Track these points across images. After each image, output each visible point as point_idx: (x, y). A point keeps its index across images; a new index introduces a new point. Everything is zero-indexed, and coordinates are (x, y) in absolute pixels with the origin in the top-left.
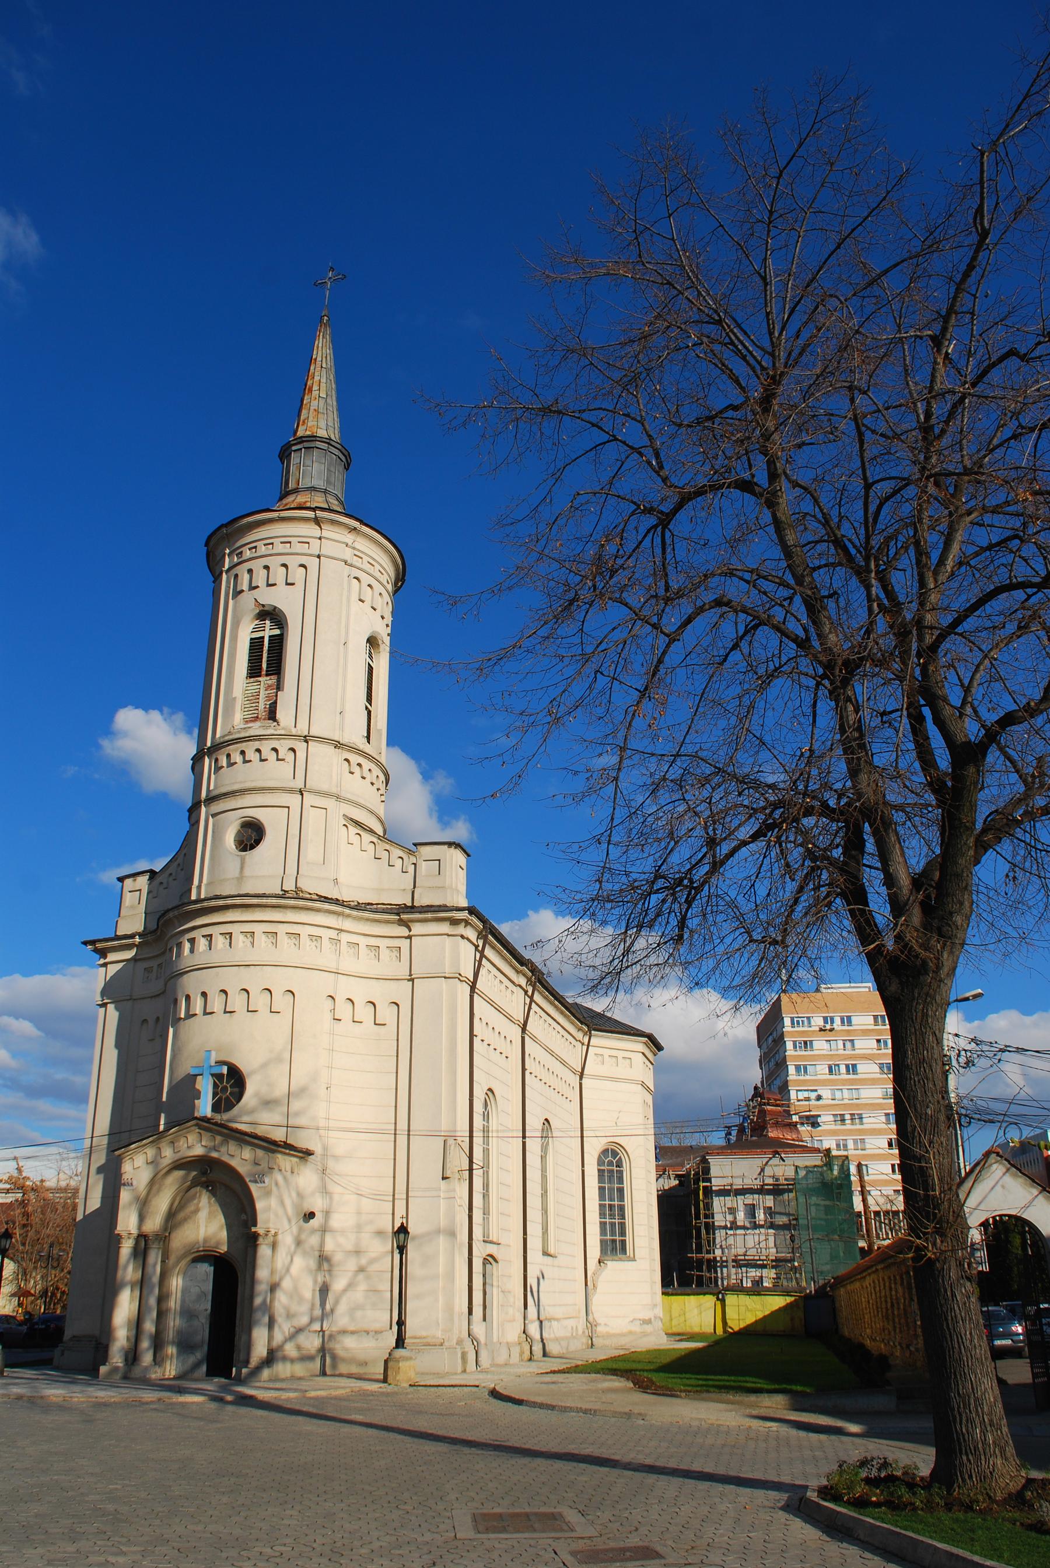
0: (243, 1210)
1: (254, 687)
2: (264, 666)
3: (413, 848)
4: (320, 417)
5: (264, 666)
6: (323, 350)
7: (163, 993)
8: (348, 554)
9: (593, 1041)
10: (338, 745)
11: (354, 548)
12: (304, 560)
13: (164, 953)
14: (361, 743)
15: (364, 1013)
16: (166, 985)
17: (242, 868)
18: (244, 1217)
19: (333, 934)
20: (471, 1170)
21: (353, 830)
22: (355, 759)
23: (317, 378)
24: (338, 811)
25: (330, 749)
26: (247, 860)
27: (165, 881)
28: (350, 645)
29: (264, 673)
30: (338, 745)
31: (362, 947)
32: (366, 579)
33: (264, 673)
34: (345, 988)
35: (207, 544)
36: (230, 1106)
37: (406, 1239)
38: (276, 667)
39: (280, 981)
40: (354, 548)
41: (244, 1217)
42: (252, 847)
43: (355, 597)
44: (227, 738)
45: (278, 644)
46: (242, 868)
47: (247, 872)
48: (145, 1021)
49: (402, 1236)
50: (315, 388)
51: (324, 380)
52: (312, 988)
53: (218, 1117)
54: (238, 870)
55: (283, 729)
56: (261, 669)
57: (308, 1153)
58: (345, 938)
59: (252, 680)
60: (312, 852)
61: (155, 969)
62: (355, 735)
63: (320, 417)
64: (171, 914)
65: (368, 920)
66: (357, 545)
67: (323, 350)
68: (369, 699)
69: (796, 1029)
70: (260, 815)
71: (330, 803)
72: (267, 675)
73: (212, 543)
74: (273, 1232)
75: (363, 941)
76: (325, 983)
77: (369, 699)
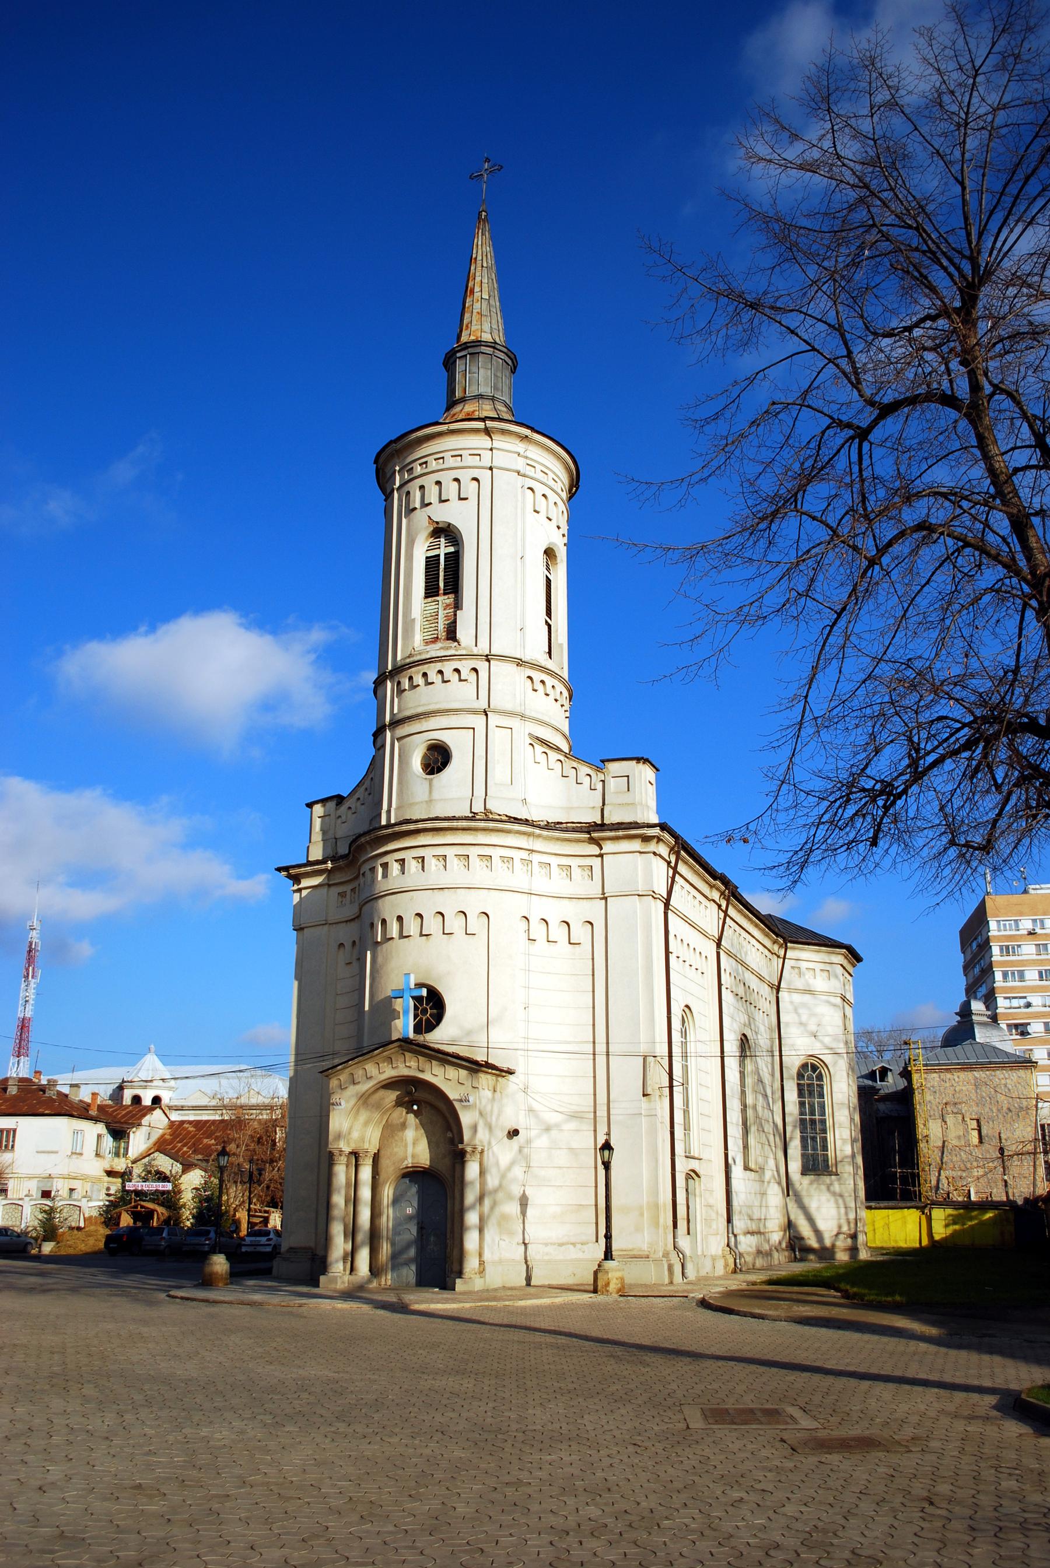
0: (449, 1128)
1: (432, 607)
2: (441, 584)
3: (601, 765)
4: (484, 322)
5: (441, 584)
6: (483, 249)
7: (358, 917)
8: (520, 464)
9: (789, 954)
10: (520, 663)
11: (526, 457)
12: (475, 473)
13: (357, 878)
14: (543, 660)
15: (558, 933)
16: (360, 910)
17: (430, 792)
18: (449, 1135)
19: (524, 855)
20: (671, 1087)
21: (539, 748)
22: (538, 676)
23: (478, 279)
24: (523, 730)
25: (512, 668)
26: (435, 782)
27: (353, 807)
28: (527, 558)
29: (441, 592)
30: (520, 663)
31: (554, 867)
32: (540, 489)
33: (441, 592)
34: (538, 909)
35: (376, 462)
36: (431, 1027)
37: (610, 1156)
38: (454, 586)
39: (473, 903)
40: (526, 457)
41: (449, 1135)
42: (439, 770)
43: (530, 508)
44: (408, 661)
45: (454, 561)
46: (430, 792)
47: (436, 795)
48: (341, 945)
49: (606, 1153)
50: (477, 289)
51: (485, 281)
52: (506, 911)
53: (420, 1038)
54: (427, 793)
55: (464, 648)
56: (438, 587)
57: (510, 1072)
58: (536, 858)
59: (430, 599)
60: (499, 773)
61: (348, 893)
62: (536, 651)
63: (484, 322)
64: (363, 840)
65: (558, 839)
66: (529, 454)
67: (483, 249)
68: (549, 613)
69: (1003, 933)
70: (445, 737)
71: (514, 722)
72: (445, 594)
73: (381, 460)
74: (480, 1149)
75: (554, 861)
76: (520, 904)
77: (549, 613)
